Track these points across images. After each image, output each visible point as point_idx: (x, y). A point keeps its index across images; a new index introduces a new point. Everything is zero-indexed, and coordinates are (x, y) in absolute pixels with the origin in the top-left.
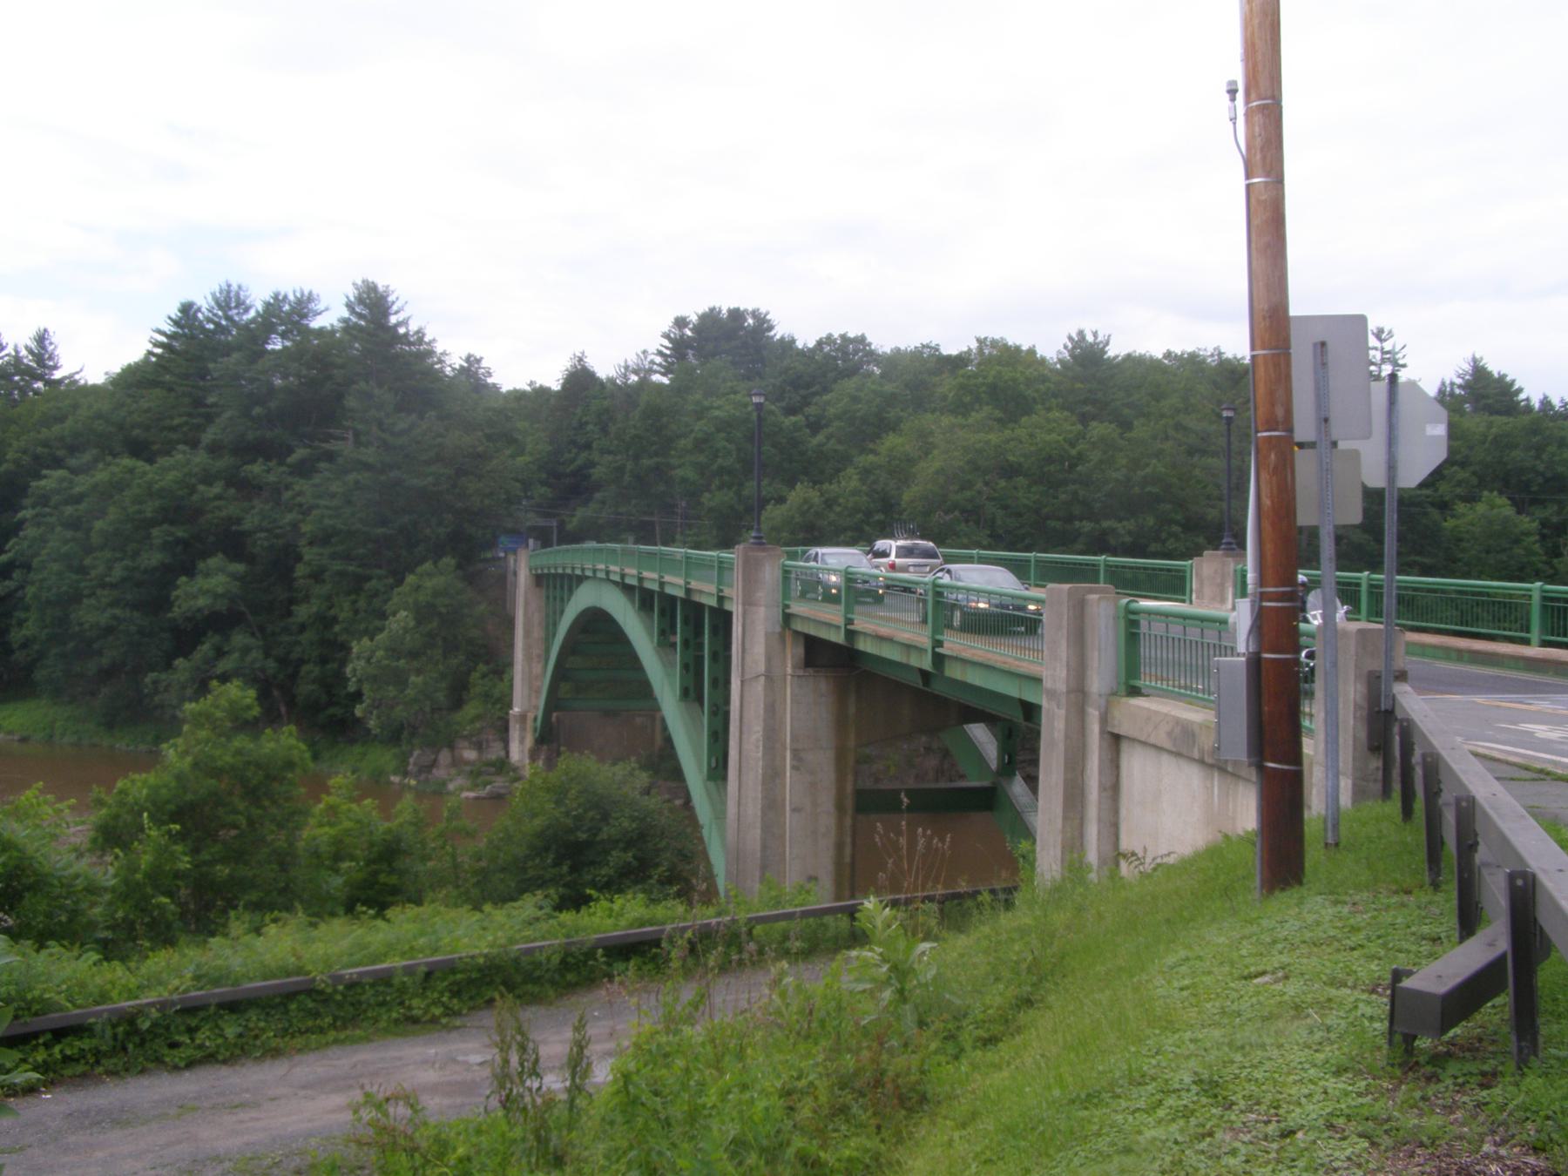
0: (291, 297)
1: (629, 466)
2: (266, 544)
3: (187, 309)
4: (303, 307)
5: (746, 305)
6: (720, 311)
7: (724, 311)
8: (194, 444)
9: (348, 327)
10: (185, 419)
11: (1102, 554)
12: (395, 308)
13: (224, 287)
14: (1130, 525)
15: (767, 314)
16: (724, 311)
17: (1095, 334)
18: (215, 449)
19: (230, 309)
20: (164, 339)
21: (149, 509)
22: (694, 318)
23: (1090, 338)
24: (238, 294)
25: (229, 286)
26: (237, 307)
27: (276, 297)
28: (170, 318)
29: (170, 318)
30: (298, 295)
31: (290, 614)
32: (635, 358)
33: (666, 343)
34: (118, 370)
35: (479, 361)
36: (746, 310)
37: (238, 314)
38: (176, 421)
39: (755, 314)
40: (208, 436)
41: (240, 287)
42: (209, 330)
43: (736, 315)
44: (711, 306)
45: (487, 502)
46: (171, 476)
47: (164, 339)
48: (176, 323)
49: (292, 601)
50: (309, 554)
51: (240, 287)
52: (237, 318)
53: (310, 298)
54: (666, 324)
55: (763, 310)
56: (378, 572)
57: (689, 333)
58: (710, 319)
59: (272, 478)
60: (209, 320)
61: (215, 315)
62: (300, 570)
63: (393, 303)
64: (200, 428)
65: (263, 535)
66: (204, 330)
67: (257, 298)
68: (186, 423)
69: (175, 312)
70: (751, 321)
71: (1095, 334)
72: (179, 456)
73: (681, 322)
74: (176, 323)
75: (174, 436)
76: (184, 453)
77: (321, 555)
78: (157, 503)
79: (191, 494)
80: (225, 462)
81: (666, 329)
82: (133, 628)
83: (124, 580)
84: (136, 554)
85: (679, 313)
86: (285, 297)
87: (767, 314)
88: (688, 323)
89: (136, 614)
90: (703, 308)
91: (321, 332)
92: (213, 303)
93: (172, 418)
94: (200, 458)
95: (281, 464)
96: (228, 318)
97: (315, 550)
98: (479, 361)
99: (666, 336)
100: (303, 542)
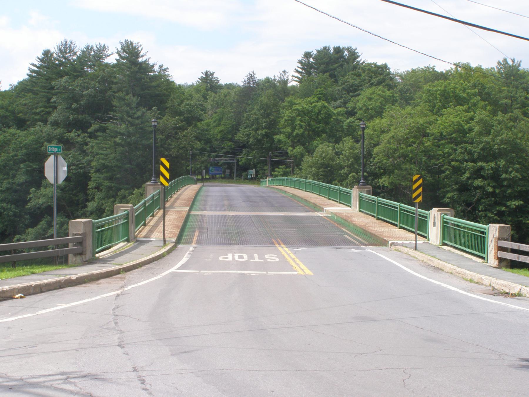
0: (95, 48)
1: (253, 133)
2: (75, 172)
3: (47, 53)
4: (101, 52)
5: (343, 44)
6: (329, 49)
7: (332, 48)
8: (45, 122)
9: (118, 64)
10: (42, 109)
11: (399, 202)
12: (141, 54)
13: (64, 42)
14: (492, 164)
15: (356, 49)
16: (332, 48)
17: (513, 61)
18: (56, 124)
19: (67, 53)
20: (36, 69)
21: (20, 154)
22: (315, 52)
23: (510, 63)
24: (70, 46)
25: (66, 42)
26: (69, 53)
27: (87, 48)
28: (38, 58)
29: (38, 58)
30: (98, 47)
31: (86, 206)
32: (279, 75)
33: (299, 65)
34: (16, 83)
35: (212, 74)
36: (344, 48)
37: (70, 56)
38: (38, 110)
39: (349, 49)
40: (52, 118)
41: (71, 42)
42: (56, 64)
43: (338, 50)
44: (324, 46)
45: (181, 151)
46: (32, 137)
47: (36, 69)
48: (42, 60)
49: (88, 201)
50: (94, 176)
51: (71, 42)
52: (70, 58)
53: (104, 48)
54: (300, 56)
55: (353, 47)
56: (126, 186)
57: (311, 60)
58: (324, 52)
59: (79, 139)
60: (57, 60)
61: (59, 56)
62: (91, 185)
63: (140, 51)
64: (49, 113)
65: (74, 167)
66: (54, 63)
67: (79, 47)
68: (43, 111)
69: (40, 55)
70: (346, 53)
71: (513, 61)
72: (37, 128)
73: (308, 55)
74: (42, 60)
75: (37, 117)
76: (40, 126)
77: (99, 177)
78: (24, 151)
79: (41, 147)
80: (59, 131)
81: (300, 59)
82: (11, 213)
83: (8, 189)
84: (14, 176)
85: (308, 50)
86: (92, 48)
87: (356, 49)
88: (312, 56)
89: (13, 206)
90: (320, 47)
91: (107, 65)
92: (58, 51)
93: (36, 108)
94: (48, 129)
95: (83, 132)
96: (66, 58)
97: (98, 175)
98: (212, 74)
99: (300, 62)
100: (93, 171)
